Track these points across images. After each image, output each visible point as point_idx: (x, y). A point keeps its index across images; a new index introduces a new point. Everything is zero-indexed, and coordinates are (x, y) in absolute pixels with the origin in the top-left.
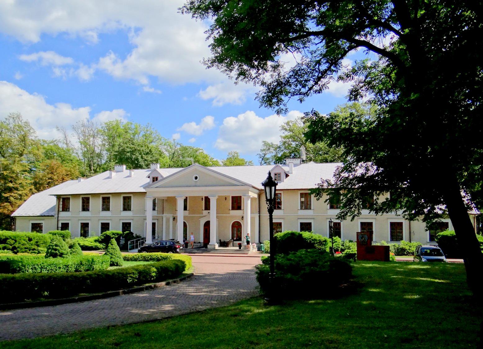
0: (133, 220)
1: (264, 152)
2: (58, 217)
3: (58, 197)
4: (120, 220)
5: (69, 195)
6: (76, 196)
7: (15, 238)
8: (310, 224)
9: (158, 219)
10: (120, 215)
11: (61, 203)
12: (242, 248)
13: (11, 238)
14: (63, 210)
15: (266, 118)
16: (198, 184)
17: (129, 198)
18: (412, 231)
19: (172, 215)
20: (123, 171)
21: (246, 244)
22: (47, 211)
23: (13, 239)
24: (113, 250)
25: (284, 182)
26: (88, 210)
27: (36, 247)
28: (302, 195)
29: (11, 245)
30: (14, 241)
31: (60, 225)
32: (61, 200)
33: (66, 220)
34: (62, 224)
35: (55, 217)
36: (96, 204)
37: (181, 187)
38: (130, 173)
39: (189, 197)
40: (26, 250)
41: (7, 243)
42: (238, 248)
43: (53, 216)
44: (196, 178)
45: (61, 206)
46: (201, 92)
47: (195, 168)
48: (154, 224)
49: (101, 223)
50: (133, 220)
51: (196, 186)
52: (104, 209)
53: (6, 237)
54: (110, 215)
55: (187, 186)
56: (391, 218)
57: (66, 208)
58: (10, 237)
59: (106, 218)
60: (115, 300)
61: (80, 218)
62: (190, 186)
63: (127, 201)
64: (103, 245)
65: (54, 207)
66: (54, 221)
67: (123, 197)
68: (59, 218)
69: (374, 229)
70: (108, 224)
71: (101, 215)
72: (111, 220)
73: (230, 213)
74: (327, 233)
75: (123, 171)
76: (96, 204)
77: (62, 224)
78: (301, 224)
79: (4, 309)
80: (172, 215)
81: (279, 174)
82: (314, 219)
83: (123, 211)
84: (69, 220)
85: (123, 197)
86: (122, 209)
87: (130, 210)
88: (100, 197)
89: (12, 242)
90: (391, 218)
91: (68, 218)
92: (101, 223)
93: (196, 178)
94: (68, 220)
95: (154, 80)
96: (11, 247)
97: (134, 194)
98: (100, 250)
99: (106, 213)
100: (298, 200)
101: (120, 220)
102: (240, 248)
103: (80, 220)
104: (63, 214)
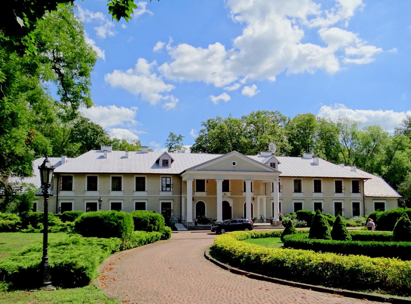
0: (147, 200)
2: (57, 196)
4: (133, 200)
5: (301, 177)
6: (129, 175)
8: (71, 204)
9: (173, 200)
10: (84, 194)
16: (236, 169)
17: (120, 179)
18: (365, 209)
21: (279, 220)
25: (171, 167)
28: (295, 181)
31: (60, 205)
33: (67, 200)
36: (104, 185)
37: (248, 171)
38: (127, 155)
39: (231, 180)
43: (52, 195)
44: (234, 164)
48: (280, 203)
50: (147, 200)
51: (234, 171)
52: (296, 191)
55: (226, 171)
59: (117, 198)
60: (232, 275)
61: (86, 198)
68: (59, 198)
70: (301, 204)
72: (123, 200)
73: (243, 195)
74: (271, 211)
76: (129, 185)
83: (87, 190)
84: (72, 200)
86: (293, 191)
87: (96, 190)
88: (160, 176)
91: (71, 198)
93: (234, 164)
94: (70, 200)
97: (125, 174)
99: (318, 195)
100: (312, 185)
101: (133, 200)
104: (63, 194)
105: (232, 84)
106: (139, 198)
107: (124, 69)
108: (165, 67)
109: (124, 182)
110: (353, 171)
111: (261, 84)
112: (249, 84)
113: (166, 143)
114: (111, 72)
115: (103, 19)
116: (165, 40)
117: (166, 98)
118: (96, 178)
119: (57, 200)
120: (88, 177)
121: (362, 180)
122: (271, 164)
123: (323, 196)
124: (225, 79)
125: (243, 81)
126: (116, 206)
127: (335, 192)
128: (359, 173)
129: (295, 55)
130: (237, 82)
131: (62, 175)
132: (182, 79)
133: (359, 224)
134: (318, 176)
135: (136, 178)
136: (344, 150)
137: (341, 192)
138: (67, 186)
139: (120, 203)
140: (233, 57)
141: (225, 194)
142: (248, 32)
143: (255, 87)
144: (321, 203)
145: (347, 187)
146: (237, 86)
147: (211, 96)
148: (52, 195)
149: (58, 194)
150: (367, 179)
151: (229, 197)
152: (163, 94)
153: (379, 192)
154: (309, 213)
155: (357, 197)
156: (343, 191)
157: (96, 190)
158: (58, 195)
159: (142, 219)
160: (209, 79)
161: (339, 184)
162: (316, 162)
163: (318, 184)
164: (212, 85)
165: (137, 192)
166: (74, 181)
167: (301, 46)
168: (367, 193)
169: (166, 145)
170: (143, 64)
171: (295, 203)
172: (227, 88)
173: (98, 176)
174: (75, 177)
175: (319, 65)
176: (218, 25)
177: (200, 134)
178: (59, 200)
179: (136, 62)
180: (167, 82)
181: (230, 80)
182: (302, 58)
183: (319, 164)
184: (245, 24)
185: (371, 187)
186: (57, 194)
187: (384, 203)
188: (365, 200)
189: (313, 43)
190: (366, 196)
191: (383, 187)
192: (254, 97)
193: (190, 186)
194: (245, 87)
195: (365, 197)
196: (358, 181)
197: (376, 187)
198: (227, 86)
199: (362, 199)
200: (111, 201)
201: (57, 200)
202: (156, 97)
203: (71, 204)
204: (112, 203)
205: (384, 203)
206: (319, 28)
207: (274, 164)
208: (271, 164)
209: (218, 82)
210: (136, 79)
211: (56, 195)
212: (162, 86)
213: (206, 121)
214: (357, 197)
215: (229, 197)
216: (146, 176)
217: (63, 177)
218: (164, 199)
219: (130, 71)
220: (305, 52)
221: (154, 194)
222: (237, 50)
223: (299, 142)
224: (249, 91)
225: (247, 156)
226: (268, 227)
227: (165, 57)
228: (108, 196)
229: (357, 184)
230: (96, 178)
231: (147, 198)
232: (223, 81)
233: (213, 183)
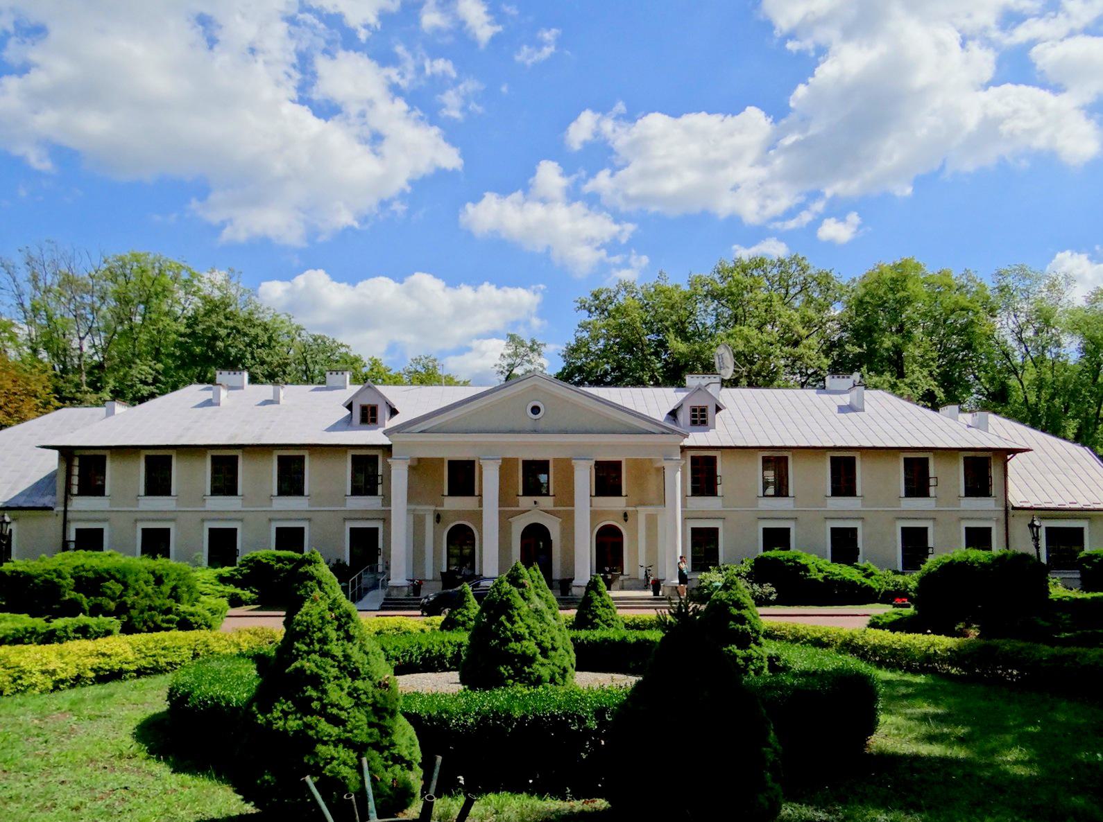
0: (309, 520)
1: (510, 361)
2: (65, 512)
3: (67, 453)
4: (270, 520)
6: (125, 452)
7: (125, 576)
8: (100, 532)
9: (384, 520)
10: (271, 506)
11: (76, 471)
12: (660, 593)
13: (113, 577)
14: (83, 492)
15: (360, 285)
16: (542, 425)
19: (433, 508)
20: (242, 388)
21: (678, 581)
22: (22, 494)
23: (118, 581)
24: (607, 611)
26: (712, 492)
27: (170, 603)
28: (767, 462)
29: (113, 599)
30: (122, 588)
31: (72, 536)
32: (76, 462)
34: (78, 531)
35: (55, 512)
38: (276, 394)
39: (555, 460)
40: (153, 612)
41: (103, 594)
42: (650, 593)
43: (51, 509)
45: (75, 480)
46: (194, 204)
47: (533, 383)
49: (143, 529)
51: (535, 431)
53: (96, 572)
54: (239, 508)
56: (968, 519)
57: (92, 484)
58: (108, 571)
61: (138, 516)
62: (519, 432)
63: (291, 468)
64: (252, 592)
65: (51, 478)
66: (52, 525)
67: (692, 457)
68: (69, 516)
69: (860, 545)
71: (207, 508)
72: (242, 520)
73: (902, 506)
75: (242, 388)
77: (78, 531)
78: (767, 531)
79: (355, 820)
80: (433, 508)
81: (703, 410)
82: (934, 519)
83: (212, 495)
84: (105, 520)
85: (692, 457)
87: (787, 495)
89: (118, 588)
90: (968, 519)
92: (143, 529)
93: (536, 410)
94: (986, 519)
95: (63, 155)
96: (112, 605)
98: (244, 607)
101: (270, 520)
102: (656, 593)
103: (142, 520)
104: (81, 504)
105: (790, 214)
106: (92, 516)
107: (503, 190)
108: (603, 181)
109: (178, 470)
110: (977, 427)
111: (869, 207)
112: (838, 210)
113: (499, 362)
114: (477, 199)
115: (454, 74)
116: (602, 108)
117: (617, 259)
118: (168, 460)
119: (65, 522)
120: (148, 458)
121: (1004, 454)
122: (694, 410)
123: (863, 506)
124: (769, 202)
125: (819, 206)
126: (156, 542)
127: (903, 494)
128: (999, 431)
129: (971, 121)
130: (802, 207)
131: (78, 452)
132: (654, 209)
133: (171, 625)
134: (839, 444)
135: (906, 460)
136: (1022, 367)
137: (925, 494)
138: (92, 484)
139: (167, 531)
140: (789, 140)
141: (535, 503)
142: (827, 71)
143: (854, 218)
144: (853, 531)
145: (949, 478)
146: (806, 217)
147: (735, 247)
148: (51, 509)
149: (69, 503)
150: (1015, 451)
151: (546, 512)
152: (613, 247)
153: (1064, 493)
154: (788, 560)
155: (982, 510)
156: (932, 491)
157: (787, 495)
158: (68, 509)
159: (37, 577)
160: (725, 205)
161: (917, 470)
162: (855, 403)
163: (843, 469)
164: (734, 220)
165: (147, 497)
166: (111, 468)
167: (983, 96)
168: (1017, 497)
169: (497, 368)
170: (550, 175)
171: (834, 530)
172: (778, 225)
173: (173, 453)
174: (177, 457)
175: (1040, 142)
176: (748, 64)
177: (578, 334)
178: (69, 521)
179: (533, 173)
180: (618, 218)
181: (783, 203)
182: (990, 127)
183: (866, 407)
184: (822, 51)
185: (1040, 478)
186: (66, 506)
187: (1081, 530)
188: (1011, 520)
189: (1027, 84)
190: (1014, 508)
191: (1084, 477)
192: (851, 244)
193: (584, 479)
194: (826, 221)
195: (1009, 510)
196: (987, 460)
197: (1062, 477)
198: (776, 219)
199: (1002, 516)
200: (208, 525)
201: (65, 522)
202: (585, 257)
203: (100, 532)
204: (144, 530)
205: (1081, 530)
206: (1032, 43)
207: (703, 410)
208: (694, 410)
209: (750, 210)
210: (536, 212)
211: (63, 509)
212: (601, 227)
213: (589, 299)
214: (982, 510)
215: (546, 512)
216: (305, 453)
217: (82, 458)
218: (368, 519)
219: (517, 196)
220: (1000, 108)
221: (327, 507)
222: (805, 121)
223: (860, 346)
224: (834, 231)
225: (582, 388)
226: (644, 603)
227: (600, 155)
228: (133, 509)
229: (982, 470)
230: (169, 458)
231: (933, 515)
232: (763, 207)
233: (567, 468)
